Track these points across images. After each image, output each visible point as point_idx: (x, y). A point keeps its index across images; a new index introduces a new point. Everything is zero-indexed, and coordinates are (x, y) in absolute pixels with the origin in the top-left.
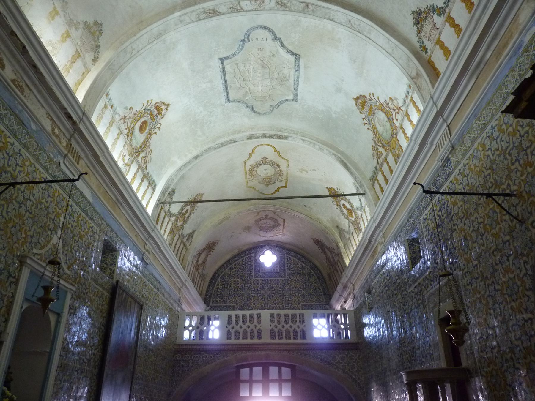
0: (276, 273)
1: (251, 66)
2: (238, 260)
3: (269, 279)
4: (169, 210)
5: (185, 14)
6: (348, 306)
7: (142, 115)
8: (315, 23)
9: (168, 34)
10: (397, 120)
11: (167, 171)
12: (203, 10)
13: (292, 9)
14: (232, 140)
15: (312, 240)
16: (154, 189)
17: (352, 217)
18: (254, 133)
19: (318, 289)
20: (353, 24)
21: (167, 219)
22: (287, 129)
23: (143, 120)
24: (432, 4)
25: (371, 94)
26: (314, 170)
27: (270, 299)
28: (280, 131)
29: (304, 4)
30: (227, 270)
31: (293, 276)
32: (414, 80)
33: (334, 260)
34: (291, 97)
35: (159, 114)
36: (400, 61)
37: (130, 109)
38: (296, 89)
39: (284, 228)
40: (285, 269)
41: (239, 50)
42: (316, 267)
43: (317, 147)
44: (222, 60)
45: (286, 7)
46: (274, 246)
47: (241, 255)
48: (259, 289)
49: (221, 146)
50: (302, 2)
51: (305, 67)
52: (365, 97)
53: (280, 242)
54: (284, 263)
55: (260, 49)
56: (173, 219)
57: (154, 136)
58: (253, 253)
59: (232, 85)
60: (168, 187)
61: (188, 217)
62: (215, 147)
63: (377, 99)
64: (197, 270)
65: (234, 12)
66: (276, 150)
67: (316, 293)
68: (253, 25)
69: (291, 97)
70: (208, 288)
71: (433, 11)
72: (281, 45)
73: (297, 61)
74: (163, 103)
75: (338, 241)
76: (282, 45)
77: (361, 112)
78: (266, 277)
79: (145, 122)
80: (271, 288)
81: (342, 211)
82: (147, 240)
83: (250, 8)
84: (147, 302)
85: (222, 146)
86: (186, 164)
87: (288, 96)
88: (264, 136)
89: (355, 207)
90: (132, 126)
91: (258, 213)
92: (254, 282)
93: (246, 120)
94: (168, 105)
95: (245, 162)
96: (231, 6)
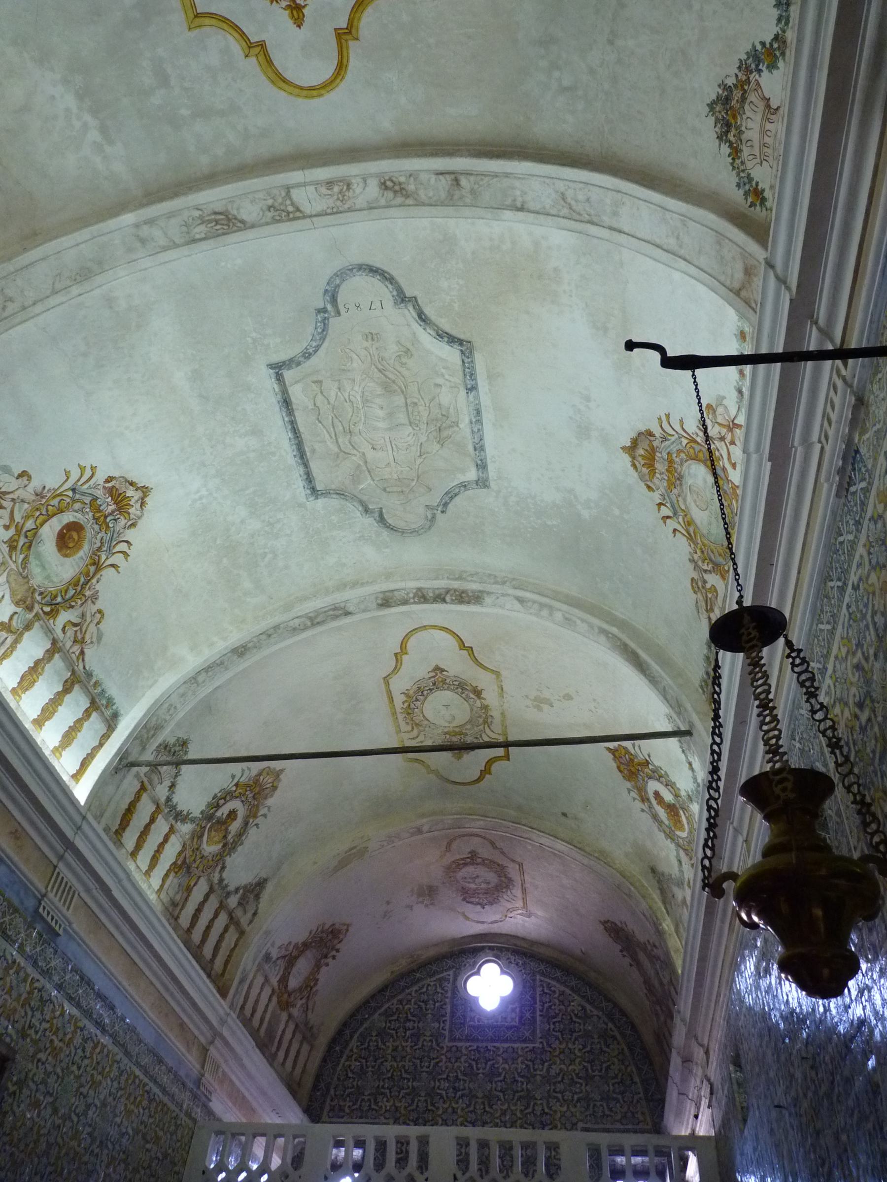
0: (511, 1027)
1: (356, 388)
2: (408, 988)
3: (490, 1046)
4: (169, 799)
5: (150, 222)
6: (704, 1127)
7: (64, 504)
8: (491, 239)
9: (111, 272)
10: (734, 466)
11: (156, 681)
12: (197, 213)
13: (423, 197)
14: (335, 609)
15: (602, 927)
16: (111, 723)
17: (682, 828)
18: (392, 586)
19: (628, 1082)
20: (573, 203)
21: (161, 826)
22: (477, 574)
23: (68, 517)
24: (749, 47)
25: (664, 418)
26: (568, 697)
27: (491, 1106)
28: (460, 578)
29: (448, 177)
30: (376, 1016)
31: (557, 1038)
32: (743, 293)
33: (661, 984)
34: (472, 474)
35: (120, 513)
36: (703, 261)
37: (20, 476)
38: (479, 447)
39: (524, 891)
40: (534, 1018)
41: (316, 340)
42: (623, 1013)
43: (558, 616)
44: (278, 369)
45: (407, 196)
46: (508, 950)
47: (418, 975)
48: (460, 1076)
49: (309, 624)
50: (442, 174)
51: (490, 377)
52: (650, 434)
53: (524, 939)
54: (534, 998)
55: (372, 337)
56: (186, 828)
57: (108, 574)
58: (450, 968)
59: (317, 446)
60: (158, 728)
61: (240, 835)
62: (291, 624)
63: (677, 428)
64: (285, 1005)
65: (278, 221)
66: (462, 645)
67: (622, 1093)
68: (338, 264)
69: (472, 474)
70: (321, 1068)
71: (757, 66)
72: (420, 316)
73: (466, 360)
74: (132, 484)
75: (659, 915)
76: (422, 317)
77: (649, 487)
78: (482, 1041)
79: (74, 527)
80: (493, 1074)
81: (655, 817)
82: (61, 858)
83: (319, 207)
84: (42, 1056)
85: (313, 625)
86: (209, 667)
87: (463, 471)
88: (422, 597)
89: (683, 793)
90: (30, 524)
91: (449, 844)
92: (449, 1055)
93: (369, 551)
94: (145, 491)
95: (386, 680)
96: (270, 202)
